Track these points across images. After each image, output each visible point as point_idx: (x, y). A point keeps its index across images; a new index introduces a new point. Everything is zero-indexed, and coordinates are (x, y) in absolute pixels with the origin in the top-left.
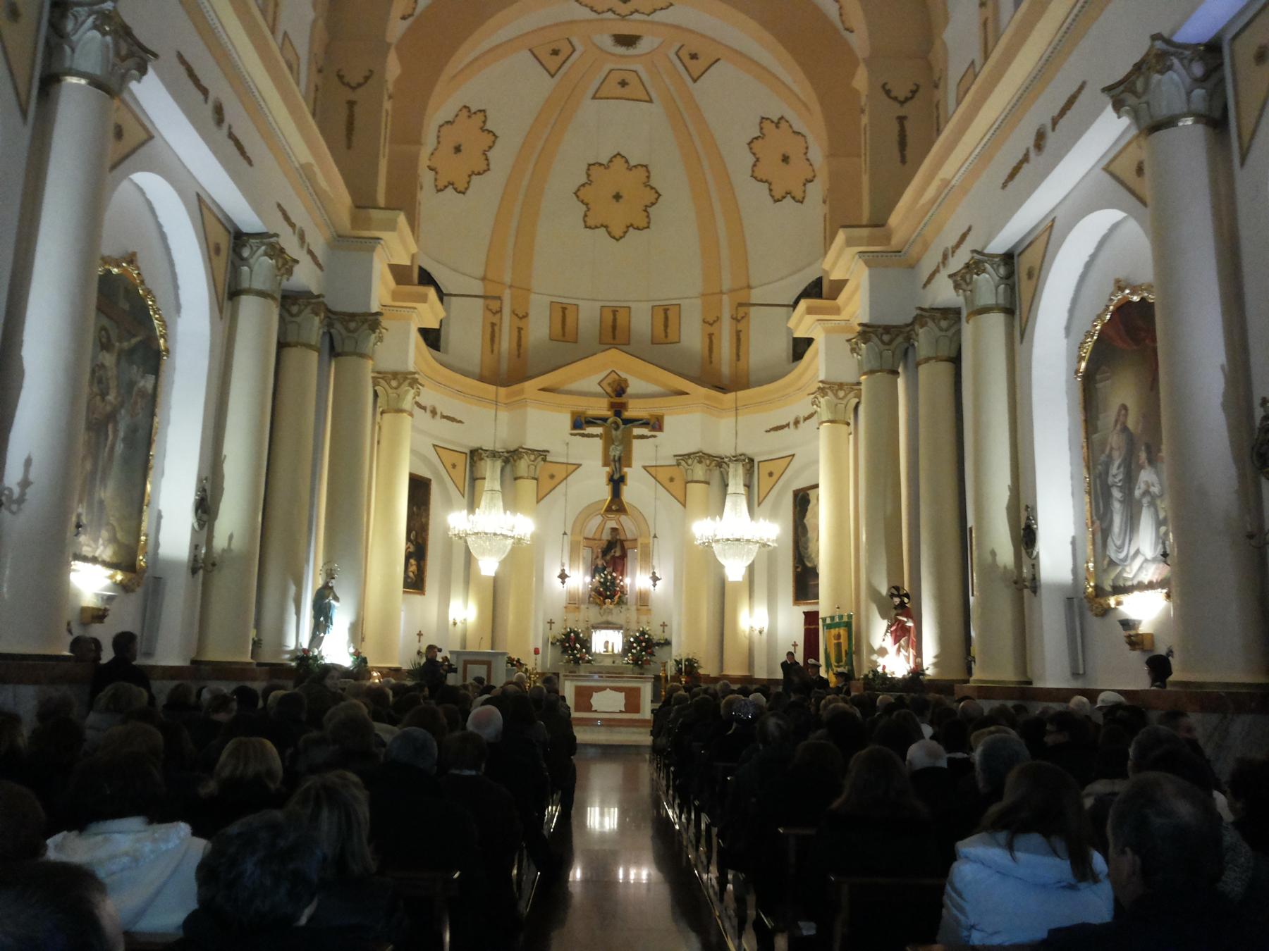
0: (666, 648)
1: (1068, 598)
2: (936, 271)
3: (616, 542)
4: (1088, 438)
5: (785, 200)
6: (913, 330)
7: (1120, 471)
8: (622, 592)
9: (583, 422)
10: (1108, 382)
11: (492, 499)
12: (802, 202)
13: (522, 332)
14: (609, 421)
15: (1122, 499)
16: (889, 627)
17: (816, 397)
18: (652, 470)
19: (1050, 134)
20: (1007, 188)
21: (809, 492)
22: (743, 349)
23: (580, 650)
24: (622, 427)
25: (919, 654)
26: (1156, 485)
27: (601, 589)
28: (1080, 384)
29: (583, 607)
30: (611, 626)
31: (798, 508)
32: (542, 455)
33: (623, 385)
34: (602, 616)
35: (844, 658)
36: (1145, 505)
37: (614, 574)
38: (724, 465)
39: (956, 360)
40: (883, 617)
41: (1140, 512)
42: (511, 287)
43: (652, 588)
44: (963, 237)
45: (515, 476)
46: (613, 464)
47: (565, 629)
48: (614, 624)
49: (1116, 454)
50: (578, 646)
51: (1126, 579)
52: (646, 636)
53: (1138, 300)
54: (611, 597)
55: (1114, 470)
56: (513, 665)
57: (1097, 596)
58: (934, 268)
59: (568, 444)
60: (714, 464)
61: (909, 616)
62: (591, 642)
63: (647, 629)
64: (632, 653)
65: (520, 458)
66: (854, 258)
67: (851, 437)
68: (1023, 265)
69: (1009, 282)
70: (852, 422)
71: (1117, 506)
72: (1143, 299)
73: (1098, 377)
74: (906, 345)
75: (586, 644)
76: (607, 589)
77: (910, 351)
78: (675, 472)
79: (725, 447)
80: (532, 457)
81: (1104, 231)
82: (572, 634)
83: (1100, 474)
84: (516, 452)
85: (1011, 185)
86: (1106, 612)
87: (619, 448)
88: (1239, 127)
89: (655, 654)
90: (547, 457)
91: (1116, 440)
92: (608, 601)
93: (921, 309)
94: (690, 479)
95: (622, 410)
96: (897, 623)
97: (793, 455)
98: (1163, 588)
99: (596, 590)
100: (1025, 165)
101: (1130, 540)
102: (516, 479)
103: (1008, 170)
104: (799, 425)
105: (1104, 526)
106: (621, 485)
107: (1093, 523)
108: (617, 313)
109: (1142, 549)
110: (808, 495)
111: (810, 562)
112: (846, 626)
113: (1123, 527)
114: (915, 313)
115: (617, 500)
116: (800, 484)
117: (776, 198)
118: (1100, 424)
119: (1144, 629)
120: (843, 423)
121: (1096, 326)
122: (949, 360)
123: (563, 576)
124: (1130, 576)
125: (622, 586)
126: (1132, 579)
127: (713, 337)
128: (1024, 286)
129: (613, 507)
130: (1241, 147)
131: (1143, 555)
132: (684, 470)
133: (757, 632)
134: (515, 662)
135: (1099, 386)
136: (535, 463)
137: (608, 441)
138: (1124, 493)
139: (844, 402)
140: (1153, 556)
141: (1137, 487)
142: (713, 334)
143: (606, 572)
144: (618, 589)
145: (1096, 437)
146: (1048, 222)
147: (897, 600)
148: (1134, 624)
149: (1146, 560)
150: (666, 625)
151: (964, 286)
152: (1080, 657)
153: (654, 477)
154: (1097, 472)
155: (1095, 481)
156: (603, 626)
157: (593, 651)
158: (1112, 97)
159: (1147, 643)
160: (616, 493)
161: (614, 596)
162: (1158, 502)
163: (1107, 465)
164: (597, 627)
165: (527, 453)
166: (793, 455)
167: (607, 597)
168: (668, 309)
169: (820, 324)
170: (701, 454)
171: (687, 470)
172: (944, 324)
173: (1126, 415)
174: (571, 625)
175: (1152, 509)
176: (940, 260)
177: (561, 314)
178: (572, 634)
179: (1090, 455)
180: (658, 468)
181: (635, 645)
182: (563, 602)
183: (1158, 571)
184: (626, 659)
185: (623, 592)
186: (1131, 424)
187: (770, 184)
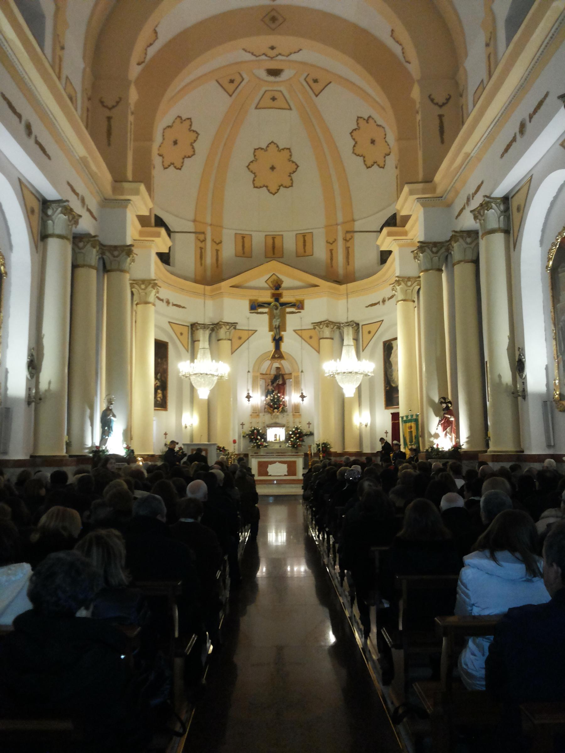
0: (311, 437)
3: (279, 376)
8: (284, 405)
11: (204, 353)
17: (394, 286)
21: (392, 342)
23: (260, 440)
24: (280, 308)
25: (458, 437)
29: (261, 414)
32: (233, 325)
34: (272, 419)
35: (414, 440)
37: (279, 395)
40: (437, 415)
43: (301, 402)
46: (275, 330)
47: (251, 427)
48: (281, 424)
50: (259, 437)
52: (299, 431)
54: (277, 408)
57: (561, 400)
58: (462, 206)
60: (335, 327)
61: (451, 414)
62: (266, 435)
64: (291, 441)
65: (221, 328)
67: (416, 309)
68: (514, 204)
70: (416, 300)
73: (559, 270)
74: (446, 254)
76: (274, 404)
78: (312, 333)
79: (342, 318)
80: (228, 327)
82: (255, 431)
84: (218, 325)
87: (278, 320)
92: (276, 410)
99: (268, 404)
102: (219, 340)
104: (385, 303)
107: (558, 357)
110: (392, 344)
115: (278, 351)
116: (387, 338)
121: (558, 239)
125: (284, 402)
127: (333, 251)
128: (515, 215)
129: (276, 356)
133: (364, 426)
137: (272, 317)
139: (411, 288)
143: (274, 394)
144: (281, 403)
146: (530, 175)
147: (444, 405)
151: (480, 217)
152: (552, 437)
154: (560, 326)
155: (559, 333)
156: (272, 425)
157: (268, 440)
165: (224, 325)
166: (383, 320)
168: (305, 235)
169: (396, 242)
171: (319, 332)
172: (469, 240)
177: (242, 240)
180: (303, 331)
182: (249, 411)
184: (288, 444)
185: (284, 405)
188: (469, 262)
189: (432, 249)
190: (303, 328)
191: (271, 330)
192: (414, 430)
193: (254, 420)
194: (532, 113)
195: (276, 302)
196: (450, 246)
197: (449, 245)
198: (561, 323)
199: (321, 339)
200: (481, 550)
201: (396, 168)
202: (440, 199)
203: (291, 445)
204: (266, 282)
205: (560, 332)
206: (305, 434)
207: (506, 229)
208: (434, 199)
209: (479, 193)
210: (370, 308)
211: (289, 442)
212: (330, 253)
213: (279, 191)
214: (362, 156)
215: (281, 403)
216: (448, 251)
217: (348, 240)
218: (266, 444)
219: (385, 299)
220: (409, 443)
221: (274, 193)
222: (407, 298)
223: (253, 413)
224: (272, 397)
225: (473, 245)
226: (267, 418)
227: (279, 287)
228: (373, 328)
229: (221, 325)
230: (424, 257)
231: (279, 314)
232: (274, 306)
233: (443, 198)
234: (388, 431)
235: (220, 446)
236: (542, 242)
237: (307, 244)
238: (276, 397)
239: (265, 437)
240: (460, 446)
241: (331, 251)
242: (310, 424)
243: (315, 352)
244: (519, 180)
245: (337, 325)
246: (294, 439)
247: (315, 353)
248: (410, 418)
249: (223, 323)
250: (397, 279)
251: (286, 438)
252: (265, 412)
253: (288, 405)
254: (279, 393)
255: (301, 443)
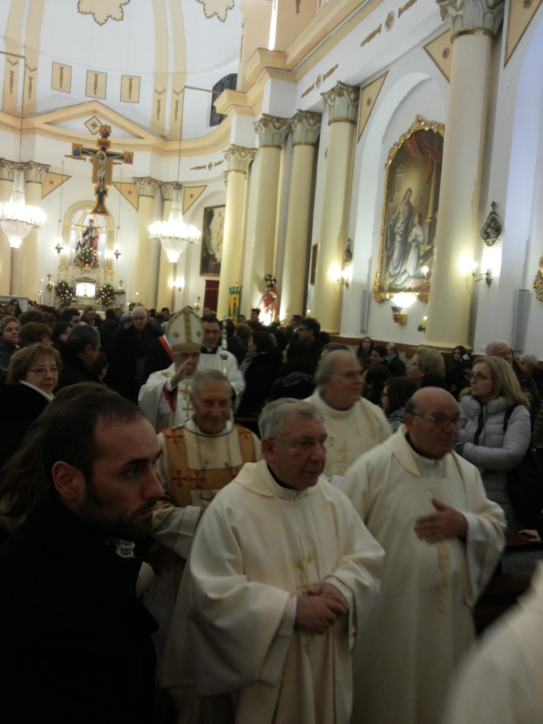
0: (122, 296)
3: (93, 228)
4: (387, 205)
6: (293, 122)
8: (95, 260)
9: (81, 152)
10: (403, 175)
11: (18, 198)
12: (224, 21)
13: (33, 81)
16: (263, 297)
18: (118, 185)
19: (396, 20)
22: (174, 109)
23: (68, 295)
24: (106, 158)
25: (278, 313)
27: (83, 258)
31: (207, 218)
32: (46, 168)
33: (108, 130)
34: (82, 274)
35: (236, 312)
37: (91, 249)
39: (316, 145)
40: (260, 291)
41: (410, 249)
42: (25, 46)
43: (115, 259)
44: (332, 70)
45: (27, 180)
46: (99, 182)
47: (59, 280)
48: (91, 279)
49: (401, 216)
50: (67, 291)
51: (397, 285)
52: (111, 288)
54: (89, 263)
55: (399, 225)
56: (32, 305)
58: (310, 86)
59: (63, 162)
60: (157, 185)
61: (274, 291)
62: (75, 290)
63: (111, 283)
65: (31, 168)
66: (263, 70)
67: (246, 181)
68: (365, 95)
69: (356, 104)
70: (247, 171)
71: (397, 245)
72: (430, 130)
73: (398, 170)
74: (287, 131)
75: (72, 291)
76: (86, 257)
77: (290, 134)
78: (131, 188)
80: (39, 168)
81: (415, 84)
82: (64, 284)
84: (28, 164)
85: (367, 45)
86: (383, 301)
87: (104, 172)
88: (507, 43)
90: (49, 169)
91: (402, 208)
92: (87, 265)
93: (301, 111)
95: (107, 147)
96: (268, 295)
98: (416, 292)
99: (79, 257)
100: (378, 34)
101: (402, 264)
102: (27, 182)
104: (211, 168)
106: (104, 196)
107: (383, 252)
109: (407, 270)
111: (211, 251)
112: (238, 293)
113: (399, 257)
115: (100, 205)
117: (207, 16)
118: (395, 197)
119: (402, 312)
121: (402, 140)
122: (312, 144)
123: (59, 249)
124: (399, 283)
125: (96, 256)
129: (99, 210)
131: (408, 273)
132: (138, 188)
134: (33, 304)
135: (397, 175)
136: (41, 173)
137: (97, 167)
138: (403, 238)
139: (245, 159)
141: (410, 236)
142: (161, 100)
143: (85, 247)
145: (391, 204)
146: (385, 71)
149: (409, 276)
151: (329, 102)
152: (366, 322)
154: (389, 224)
155: (387, 229)
156: (83, 280)
157: (77, 294)
158: (441, 6)
160: (101, 201)
161: (91, 262)
162: (421, 246)
163: (396, 222)
167: (86, 263)
168: (132, 79)
169: (235, 107)
171: (140, 188)
173: (410, 196)
174: (63, 278)
175: (417, 249)
176: (315, 81)
177: (60, 71)
178: (64, 284)
179: (387, 213)
181: (103, 293)
182: (57, 263)
184: (98, 301)
185: (96, 260)
186: (412, 200)
187: (204, 5)
189: (275, 124)
190: (123, 181)
191: (94, 181)
192: (237, 301)
193: (63, 274)
194: (402, 7)
195: (102, 151)
196: (293, 124)
197: (291, 122)
202: (289, 72)
203: (102, 302)
204: (85, 124)
205: (389, 229)
206: (117, 292)
207: (353, 119)
208: (275, 70)
210: (194, 170)
211: (100, 298)
212: (157, 104)
213: (107, 22)
214: (202, 3)
215: (93, 258)
217: (179, 92)
218: (75, 299)
219: (211, 164)
220: (232, 314)
221: (101, 23)
223: (61, 265)
225: (315, 128)
226: (75, 272)
227: (106, 135)
228: (196, 192)
229: (31, 165)
230: (266, 130)
231: (105, 165)
232: (100, 155)
233: (291, 72)
234: (200, 297)
235: (31, 300)
240: (280, 322)
245: (159, 184)
246: (105, 297)
247: (135, 210)
248: (235, 290)
250: (232, 147)
252: (75, 265)
253: (99, 260)
255: (112, 301)
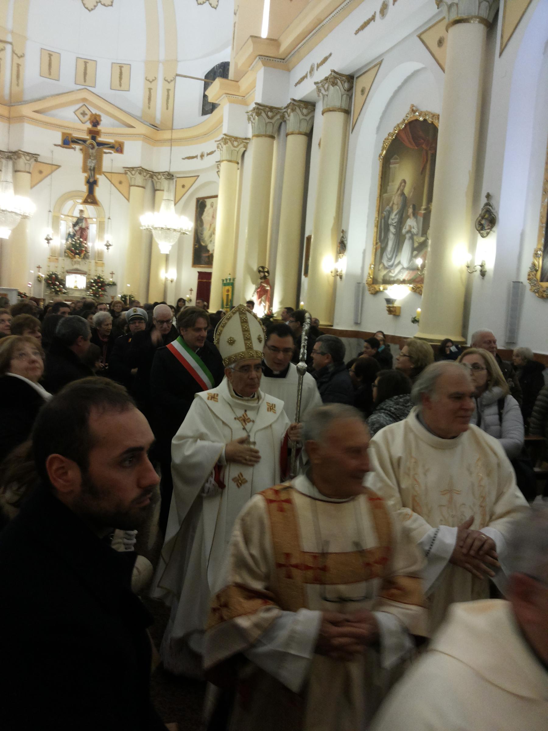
0: (114, 287)
1: (358, 283)
2: (305, 77)
3: (83, 219)
4: (381, 196)
5: (204, 4)
7: (396, 217)
10: (397, 165)
14: (88, 142)
15: (395, 233)
16: (257, 289)
17: (220, 144)
20: (358, 35)
21: (206, 200)
24: (96, 147)
25: (271, 305)
26: (415, 228)
28: (381, 162)
29: (60, 259)
30: (78, 272)
31: (199, 209)
32: (34, 157)
33: (98, 119)
34: (73, 265)
36: (407, 238)
37: (81, 240)
38: (155, 177)
39: (309, 135)
40: (253, 283)
43: (106, 250)
44: (326, 59)
46: (89, 172)
48: (83, 271)
49: (395, 207)
50: (57, 283)
53: (422, 120)
54: (79, 254)
55: (393, 216)
57: (373, 283)
58: (304, 74)
60: (148, 175)
61: (268, 283)
62: (65, 281)
64: (93, 290)
67: (239, 171)
68: (359, 85)
69: (350, 94)
70: (240, 162)
71: (391, 237)
72: (425, 120)
73: (392, 161)
74: (281, 121)
75: (62, 282)
76: (76, 248)
78: (122, 178)
79: (161, 166)
81: (409, 73)
83: (385, 217)
85: (361, 33)
86: (376, 293)
87: (94, 161)
89: (106, 290)
91: (396, 199)
92: (77, 256)
93: (294, 100)
94: (133, 184)
95: (97, 136)
97: (198, 176)
98: (410, 284)
99: (69, 249)
100: (372, 22)
101: (396, 256)
103: (361, 23)
105: (383, 246)
107: (377, 244)
108: (87, 64)
109: (402, 262)
110: (205, 202)
111: (204, 242)
114: (289, 101)
116: (202, 194)
118: (389, 188)
119: (396, 304)
120: (235, 163)
122: (305, 134)
124: (393, 275)
126: (394, 277)
127: (152, 91)
128: (357, 97)
130: (502, 44)
133: (169, 282)
135: (391, 166)
137: (87, 157)
139: (237, 149)
140: (407, 266)
141: (404, 227)
143: (76, 238)
144: (84, 249)
145: (385, 195)
147: (262, 274)
148: (392, 301)
149: (403, 268)
150: (114, 274)
151: (323, 91)
153: (109, 180)
154: (383, 215)
155: (381, 219)
159: (397, 311)
160: (91, 191)
162: (415, 237)
163: (390, 212)
164: (70, 272)
165: (24, 155)
166: (198, 176)
167: (76, 254)
169: (227, 96)
170: (141, 168)
171: (131, 178)
172: (305, 111)
173: (404, 186)
174: (53, 270)
177: (48, 59)
180: (113, 174)
181: (94, 284)
182: (47, 254)
183: (409, 275)
185: (87, 252)
186: (406, 191)
188: (303, 134)
193: (53, 265)
196: (286, 113)
197: (285, 112)
198: (385, 213)
199: (132, 186)
200: (246, 398)
201: (235, 14)
205: (383, 221)
209: (325, 65)
210: (187, 160)
216: (284, 120)
217: (170, 81)
218: (65, 291)
222: (232, 159)
223: (52, 256)
224: (73, 241)
225: (308, 118)
226: (65, 263)
231: (95, 154)
232: (90, 144)
233: (284, 61)
236: (378, 128)
237: (124, 76)
238: (78, 241)
239: (64, 283)
241: (150, 89)
242: (114, 274)
243: (126, 200)
244: (366, 63)
249: (22, 153)
250: (225, 137)
251: (87, 286)
253: (90, 252)
254: (81, 237)
